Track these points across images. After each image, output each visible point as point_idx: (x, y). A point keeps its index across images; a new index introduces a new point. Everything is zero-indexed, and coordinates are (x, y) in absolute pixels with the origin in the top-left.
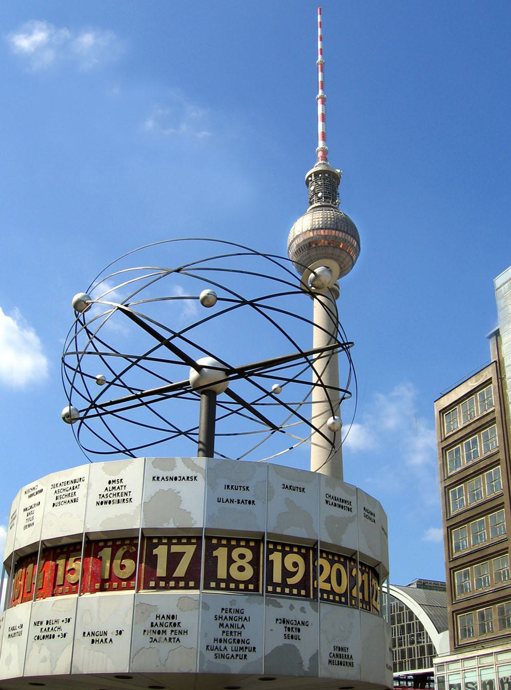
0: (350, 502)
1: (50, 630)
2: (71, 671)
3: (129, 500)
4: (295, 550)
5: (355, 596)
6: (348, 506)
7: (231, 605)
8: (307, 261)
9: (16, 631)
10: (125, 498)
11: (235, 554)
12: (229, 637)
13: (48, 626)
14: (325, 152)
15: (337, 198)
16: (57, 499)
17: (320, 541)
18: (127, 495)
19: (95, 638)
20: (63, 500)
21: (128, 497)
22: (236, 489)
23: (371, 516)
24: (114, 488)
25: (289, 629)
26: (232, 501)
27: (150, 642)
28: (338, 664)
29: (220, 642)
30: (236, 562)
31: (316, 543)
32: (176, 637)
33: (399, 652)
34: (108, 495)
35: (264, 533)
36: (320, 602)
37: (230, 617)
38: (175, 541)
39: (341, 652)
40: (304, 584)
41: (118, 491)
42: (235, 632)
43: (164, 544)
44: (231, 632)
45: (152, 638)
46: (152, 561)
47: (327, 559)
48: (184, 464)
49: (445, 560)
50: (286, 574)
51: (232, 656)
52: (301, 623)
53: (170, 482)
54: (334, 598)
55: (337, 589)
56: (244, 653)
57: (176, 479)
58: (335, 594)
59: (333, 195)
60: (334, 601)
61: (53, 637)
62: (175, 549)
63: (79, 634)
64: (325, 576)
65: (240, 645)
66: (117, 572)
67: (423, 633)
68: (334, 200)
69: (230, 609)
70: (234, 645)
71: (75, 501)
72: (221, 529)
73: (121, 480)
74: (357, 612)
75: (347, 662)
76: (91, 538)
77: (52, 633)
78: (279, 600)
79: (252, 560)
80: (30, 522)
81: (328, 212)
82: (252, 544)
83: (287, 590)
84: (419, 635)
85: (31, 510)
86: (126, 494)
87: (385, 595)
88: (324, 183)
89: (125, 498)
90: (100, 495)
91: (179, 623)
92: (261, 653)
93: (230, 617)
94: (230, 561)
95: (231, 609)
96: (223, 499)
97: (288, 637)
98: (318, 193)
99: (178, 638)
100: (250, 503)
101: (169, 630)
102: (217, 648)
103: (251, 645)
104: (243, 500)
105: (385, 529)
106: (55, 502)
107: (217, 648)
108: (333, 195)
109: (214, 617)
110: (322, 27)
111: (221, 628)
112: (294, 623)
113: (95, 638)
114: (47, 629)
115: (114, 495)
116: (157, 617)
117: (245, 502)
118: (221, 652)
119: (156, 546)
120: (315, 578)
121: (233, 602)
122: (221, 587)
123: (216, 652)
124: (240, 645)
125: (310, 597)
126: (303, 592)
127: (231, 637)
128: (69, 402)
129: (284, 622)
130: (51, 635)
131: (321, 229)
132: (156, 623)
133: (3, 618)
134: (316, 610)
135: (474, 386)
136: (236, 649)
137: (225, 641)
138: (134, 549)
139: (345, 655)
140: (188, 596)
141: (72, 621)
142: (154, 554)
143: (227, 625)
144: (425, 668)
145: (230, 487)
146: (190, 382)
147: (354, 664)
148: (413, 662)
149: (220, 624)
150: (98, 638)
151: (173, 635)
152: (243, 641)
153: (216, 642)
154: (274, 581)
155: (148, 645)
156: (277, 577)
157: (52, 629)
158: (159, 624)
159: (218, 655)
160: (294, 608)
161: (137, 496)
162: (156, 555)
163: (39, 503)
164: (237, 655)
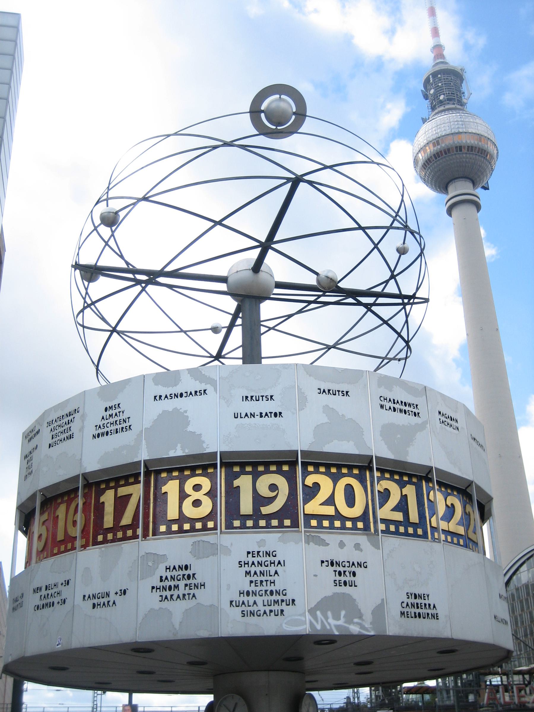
1: (49, 596)
3: (128, 428)
5: (436, 526)
6: (414, 410)
12: (258, 589)
15: (463, 97)
17: (376, 456)
18: (125, 422)
19: (96, 601)
21: (128, 424)
22: (256, 400)
24: (111, 416)
26: (252, 415)
27: (160, 601)
31: (371, 461)
32: (192, 592)
35: (372, 456)
36: (382, 536)
39: (418, 601)
42: (267, 581)
44: (261, 582)
48: (191, 376)
49: (6, 253)
51: (265, 612)
55: (346, 511)
56: (280, 608)
61: (53, 606)
65: (275, 597)
69: (258, 552)
70: (266, 598)
71: (71, 437)
73: (119, 404)
74: (437, 546)
75: (428, 614)
78: (322, 536)
86: (125, 421)
90: (96, 426)
91: (194, 575)
93: (258, 562)
94: (183, 496)
95: (259, 552)
97: (340, 583)
98: (440, 96)
99: (194, 594)
101: (182, 584)
102: (243, 603)
103: (289, 597)
104: (266, 413)
107: (243, 603)
111: (248, 576)
112: (347, 564)
113: (96, 601)
115: (111, 424)
116: (167, 569)
117: (269, 415)
118: (249, 609)
123: (243, 608)
124: (275, 597)
125: (371, 531)
130: (50, 603)
132: (166, 576)
134: (376, 546)
136: (269, 604)
137: (254, 594)
139: (425, 605)
143: (255, 573)
145: (249, 398)
147: (439, 615)
149: (246, 572)
152: (278, 593)
153: (242, 595)
157: (52, 595)
158: (169, 578)
159: (245, 613)
160: (345, 545)
164: (271, 611)
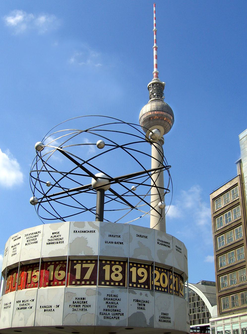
0: (169, 243)
1: (24, 305)
2: (34, 325)
3: (62, 242)
4: (143, 266)
5: (172, 289)
6: (168, 245)
7: (112, 293)
8: (148, 126)
9: (7, 306)
10: (60, 241)
11: (114, 268)
12: (110, 309)
13: (23, 303)
14: (157, 73)
15: (163, 96)
16: (27, 242)
17: (155, 262)
18: (61, 240)
19: (46, 309)
20: (30, 242)
21: (62, 241)
22: (114, 237)
23: (179, 250)
24: (55, 236)
25: (140, 304)
26: (112, 243)
27: (73, 311)
28: (164, 322)
29: (107, 311)
30: (114, 272)
31: (153, 263)
32: (85, 308)
33: (193, 315)
34: (52, 240)
35: (128, 258)
36: (155, 291)
37: (111, 299)
38: (84, 262)
39: (165, 316)
40: (147, 282)
41: (57, 238)
42: (114, 306)
43: (80, 263)
44: (112, 306)
45: (73, 309)
46: (73, 272)
47: (158, 270)
48: (89, 225)
49: (215, 271)
50: (138, 278)
51: (112, 318)
52: (145, 301)
53: (82, 233)
54: (162, 289)
56: (118, 316)
57: (85, 232)
58: (162, 287)
59: (161, 94)
60: (161, 291)
61: (26, 309)
62: (85, 266)
63: (38, 307)
64: (157, 279)
65: (116, 312)
66: (57, 277)
67: (205, 306)
68: (161, 97)
69: (111, 295)
70: (113, 312)
71: (36, 242)
72: (107, 256)
73: (59, 232)
74: (172, 296)
75: (168, 321)
76: (44, 260)
77: (25, 306)
78: (135, 290)
79: (122, 271)
80: (14, 253)
81: (159, 102)
82: (122, 263)
83: (139, 286)
84: (203, 308)
85: (15, 247)
86: (61, 239)
87: (186, 288)
88: (157, 89)
89: (60, 241)
90: (48, 240)
91: (86, 302)
92: (126, 316)
93: (111, 299)
94: (111, 272)
95: (112, 295)
96: (108, 241)
97: (139, 308)
98: (154, 93)
99: (86, 309)
100: (121, 243)
101: (82, 305)
102: (105, 314)
103: (121, 312)
104: (117, 242)
105: (186, 256)
106: (27, 243)
107: (105, 314)
108: (161, 94)
109: (103, 299)
110: (156, 13)
111: (107, 304)
112: (142, 301)
113: (46, 309)
114: (23, 305)
115: (55, 240)
116: (76, 299)
117: (118, 243)
118: (107, 316)
119: (75, 264)
120: (152, 280)
121: (113, 291)
122: (107, 284)
123: (105, 315)
124: (116, 312)
125: (150, 289)
126: (146, 287)
127: (112, 308)
128: (33, 195)
129: (137, 301)
130: (24, 307)
131: (155, 111)
132: (76, 302)
133: (1, 299)
134: (153, 295)
135: (229, 187)
136: (114, 314)
137: (109, 310)
138: (65, 266)
139: (167, 317)
140: (91, 289)
141: (35, 301)
142: (74, 268)
143: (110, 303)
144: (205, 323)
145: (111, 236)
146: (92, 185)
147: (171, 321)
148: (200, 321)
149: (106, 302)
150: (47, 309)
151: (84, 308)
152: (118, 311)
153: (104, 311)
154: (132, 281)
155: (71, 312)
156: (134, 279)
157: (25, 305)
158: (77, 302)
159: (105, 317)
160: (142, 294)
161: (66, 240)
162: (76, 269)
163: (19, 243)
164: (115, 317)
